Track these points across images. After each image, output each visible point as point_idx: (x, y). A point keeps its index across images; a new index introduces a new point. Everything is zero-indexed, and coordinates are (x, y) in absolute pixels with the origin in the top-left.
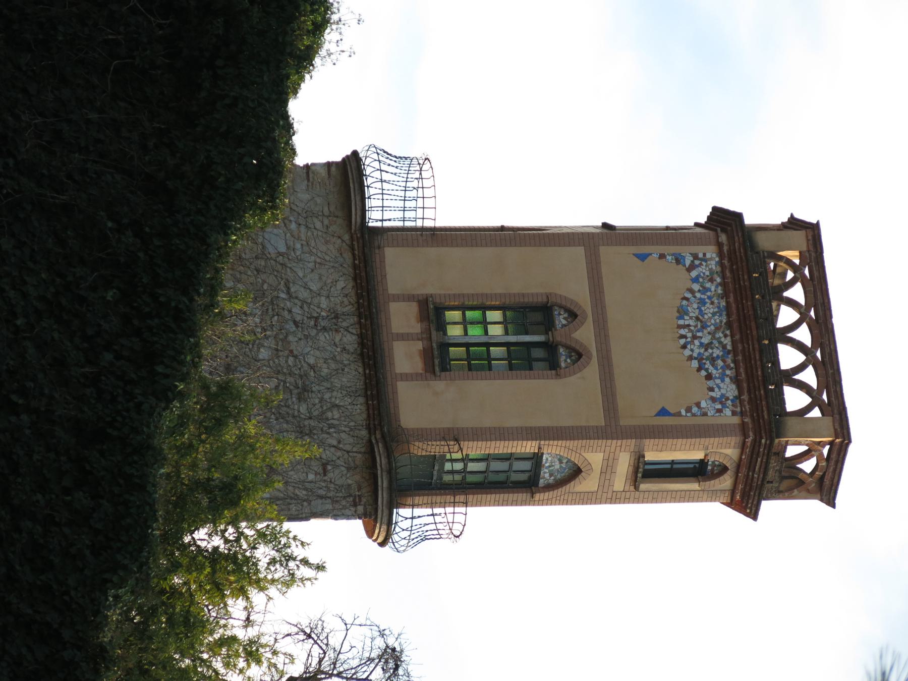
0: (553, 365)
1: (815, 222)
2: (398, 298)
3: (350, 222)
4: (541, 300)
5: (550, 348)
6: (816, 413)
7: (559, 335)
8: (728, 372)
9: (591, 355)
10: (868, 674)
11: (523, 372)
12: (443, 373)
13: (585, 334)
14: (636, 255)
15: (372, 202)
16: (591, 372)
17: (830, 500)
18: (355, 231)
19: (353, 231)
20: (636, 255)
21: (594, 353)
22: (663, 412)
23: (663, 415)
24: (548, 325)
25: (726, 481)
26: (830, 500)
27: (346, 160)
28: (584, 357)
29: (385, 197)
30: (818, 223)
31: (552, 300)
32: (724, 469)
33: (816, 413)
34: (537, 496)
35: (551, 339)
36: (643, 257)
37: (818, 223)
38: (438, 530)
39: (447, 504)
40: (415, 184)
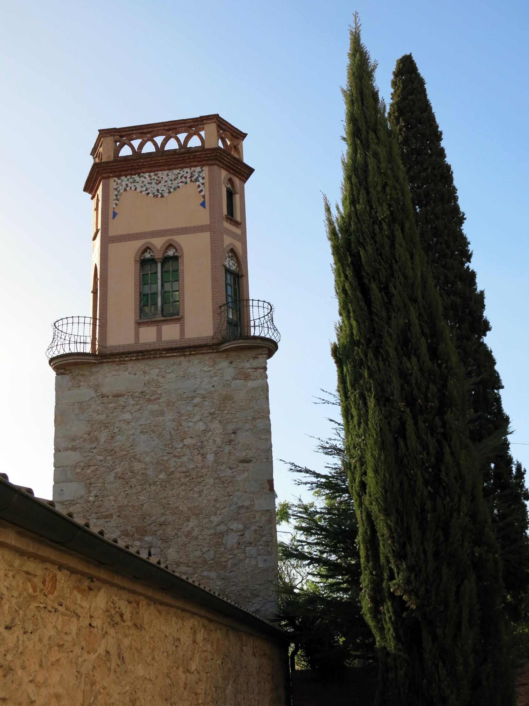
0: (175, 258)
1: (98, 133)
2: (137, 335)
3: (93, 363)
4: (138, 265)
5: (166, 260)
6: (202, 133)
7: (158, 256)
8: (123, 653)
9: (170, 239)
10: (344, 92)
11: (180, 265)
12: (180, 314)
13: (158, 243)
14: (114, 218)
15: (80, 349)
16: (180, 239)
17: (244, 135)
18: (97, 360)
19: (97, 362)
20: (114, 218)
21: (169, 238)
22: (203, 204)
23: (205, 204)
24: (152, 261)
25: (237, 181)
26: (244, 135)
27: (56, 369)
28: (171, 243)
29: (78, 341)
30: (99, 131)
31: (138, 259)
32: (230, 181)
33: (202, 133)
34: (244, 274)
35: (161, 260)
36: (115, 215)
37: (99, 131)
38: (267, 322)
39: (248, 324)
40: (72, 339)
